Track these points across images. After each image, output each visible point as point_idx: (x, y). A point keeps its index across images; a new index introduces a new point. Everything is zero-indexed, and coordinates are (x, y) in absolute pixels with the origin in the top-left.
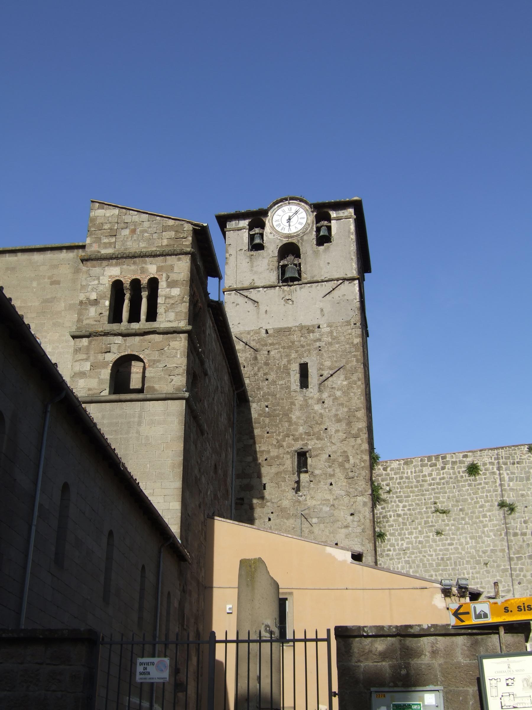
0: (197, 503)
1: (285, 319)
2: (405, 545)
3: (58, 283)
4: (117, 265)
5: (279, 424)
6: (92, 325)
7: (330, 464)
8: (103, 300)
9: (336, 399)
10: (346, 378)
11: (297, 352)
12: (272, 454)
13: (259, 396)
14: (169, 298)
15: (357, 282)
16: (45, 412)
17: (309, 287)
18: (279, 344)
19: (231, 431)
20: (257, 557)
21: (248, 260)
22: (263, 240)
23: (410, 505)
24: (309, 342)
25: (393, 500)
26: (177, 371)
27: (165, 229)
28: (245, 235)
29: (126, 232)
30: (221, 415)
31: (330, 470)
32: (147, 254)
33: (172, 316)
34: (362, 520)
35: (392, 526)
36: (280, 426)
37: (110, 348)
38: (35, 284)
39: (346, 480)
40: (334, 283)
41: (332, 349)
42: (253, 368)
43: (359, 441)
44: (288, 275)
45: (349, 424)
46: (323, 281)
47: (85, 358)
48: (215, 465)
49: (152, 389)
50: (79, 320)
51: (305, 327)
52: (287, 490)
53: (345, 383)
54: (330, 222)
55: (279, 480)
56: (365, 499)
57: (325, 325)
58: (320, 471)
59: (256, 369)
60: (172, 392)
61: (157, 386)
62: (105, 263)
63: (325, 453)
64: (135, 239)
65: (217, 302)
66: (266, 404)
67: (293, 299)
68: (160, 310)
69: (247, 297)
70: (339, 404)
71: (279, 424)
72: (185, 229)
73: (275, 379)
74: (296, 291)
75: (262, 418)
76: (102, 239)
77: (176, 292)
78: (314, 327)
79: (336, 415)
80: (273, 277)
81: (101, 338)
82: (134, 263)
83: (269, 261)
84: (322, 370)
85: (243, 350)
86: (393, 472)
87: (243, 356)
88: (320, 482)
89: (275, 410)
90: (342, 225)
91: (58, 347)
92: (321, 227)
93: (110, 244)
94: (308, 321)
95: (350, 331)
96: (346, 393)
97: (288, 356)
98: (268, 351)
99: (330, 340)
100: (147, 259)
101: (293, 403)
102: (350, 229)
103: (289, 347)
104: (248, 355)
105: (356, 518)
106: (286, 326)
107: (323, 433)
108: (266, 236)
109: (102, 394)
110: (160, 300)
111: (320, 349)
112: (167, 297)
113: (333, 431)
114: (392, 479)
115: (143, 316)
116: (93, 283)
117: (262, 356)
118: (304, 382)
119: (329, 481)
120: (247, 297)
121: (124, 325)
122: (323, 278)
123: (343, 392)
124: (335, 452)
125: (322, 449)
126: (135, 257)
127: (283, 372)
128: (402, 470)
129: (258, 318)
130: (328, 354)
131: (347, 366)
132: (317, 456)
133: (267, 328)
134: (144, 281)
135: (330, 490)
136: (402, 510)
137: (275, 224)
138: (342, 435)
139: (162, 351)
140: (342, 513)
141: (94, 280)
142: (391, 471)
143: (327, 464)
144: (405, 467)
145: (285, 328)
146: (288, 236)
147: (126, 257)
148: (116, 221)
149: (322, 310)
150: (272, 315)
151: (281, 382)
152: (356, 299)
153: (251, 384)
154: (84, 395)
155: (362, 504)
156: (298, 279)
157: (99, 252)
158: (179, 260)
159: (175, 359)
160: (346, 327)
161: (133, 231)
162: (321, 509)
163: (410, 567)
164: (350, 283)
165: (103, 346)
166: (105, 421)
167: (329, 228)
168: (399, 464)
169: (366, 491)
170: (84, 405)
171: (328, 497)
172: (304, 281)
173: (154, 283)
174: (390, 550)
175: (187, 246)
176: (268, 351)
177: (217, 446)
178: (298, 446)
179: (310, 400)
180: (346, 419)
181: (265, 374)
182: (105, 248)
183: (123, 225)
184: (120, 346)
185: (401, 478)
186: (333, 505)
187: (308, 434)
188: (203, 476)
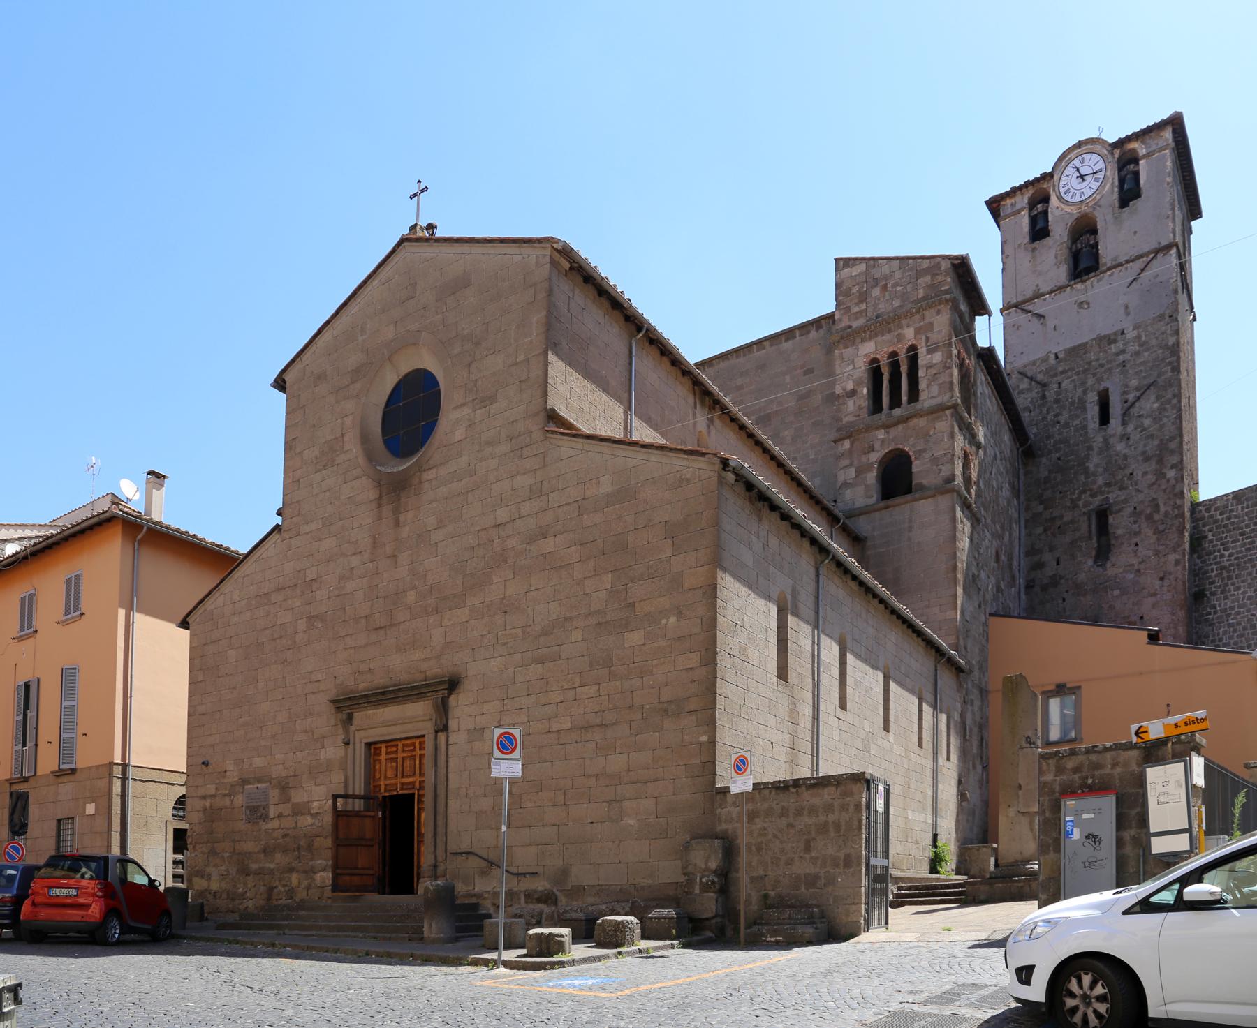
0: (976, 604)
2: (1229, 605)
11: (1094, 375)
12: (1065, 519)
23: (1238, 552)
27: (920, 274)
29: (876, 292)
31: (1135, 527)
38: (788, 378)
44: (1082, 266)
46: (1128, 262)
47: (835, 648)
51: (1105, 337)
53: (1156, 405)
61: (925, 482)
65: (988, 349)
68: (922, 385)
77: (937, 357)
93: (861, 312)
94: (1106, 327)
96: (1156, 420)
97: (1083, 384)
101: (1090, 448)
102: (1165, 166)
103: (1085, 371)
105: (1166, 582)
110: (921, 373)
112: (929, 367)
113: (1140, 474)
115: (904, 398)
118: (1104, 419)
121: (883, 416)
124: (1142, 502)
125: (1125, 501)
127: (1077, 409)
132: (1119, 511)
137: (1062, 190)
151: (1076, 422)
157: (850, 327)
158: (938, 312)
161: (885, 288)
171: (1134, 561)
178: (1097, 501)
181: (1056, 416)
182: (857, 319)
184: (883, 441)
186: (1138, 571)
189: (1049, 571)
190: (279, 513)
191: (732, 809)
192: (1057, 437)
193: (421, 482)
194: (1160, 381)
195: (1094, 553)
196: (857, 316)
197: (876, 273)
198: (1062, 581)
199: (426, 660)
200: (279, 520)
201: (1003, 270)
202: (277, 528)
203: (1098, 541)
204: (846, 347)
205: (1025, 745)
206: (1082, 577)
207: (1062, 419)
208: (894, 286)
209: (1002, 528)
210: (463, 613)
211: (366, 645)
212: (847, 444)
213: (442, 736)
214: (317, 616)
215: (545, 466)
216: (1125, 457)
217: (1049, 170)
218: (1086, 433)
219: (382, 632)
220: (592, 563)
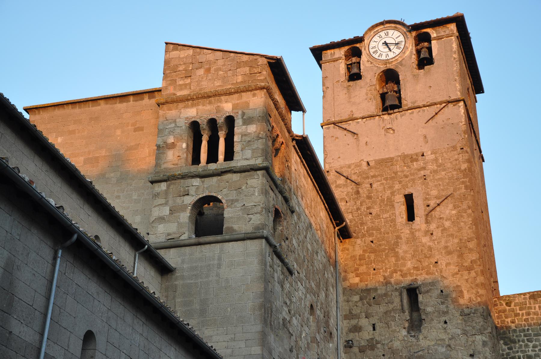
0: (287, 347)
1: (386, 150)
3: (141, 129)
4: (193, 106)
5: (385, 259)
6: (170, 169)
7: (443, 301)
8: (180, 143)
9: (444, 230)
10: (455, 207)
11: (400, 182)
12: (379, 292)
13: (363, 231)
14: (245, 135)
15: (462, 103)
16: (55, 258)
17: (410, 114)
18: (381, 175)
19: (332, 269)
21: (345, 91)
22: (360, 69)
24: (412, 171)
25: (521, 339)
27: (239, 65)
28: (342, 66)
29: (201, 72)
30: (317, 253)
31: (443, 307)
32: (222, 93)
33: (248, 153)
36: (386, 261)
37: (188, 190)
38: (118, 132)
39: (461, 317)
40: (437, 108)
41: (438, 177)
42: (356, 202)
43: (473, 274)
45: (461, 256)
46: (424, 106)
47: (163, 202)
48: (312, 306)
49: (231, 229)
50: (157, 165)
51: (408, 156)
52: (398, 330)
53: (454, 212)
54: (431, 43)
55: (389, 319)
56: (484, 338)
57: (429, 153)
58: (433, 308)
59: (358, 203)
60: (250, 232)
61: (236, 227)
62: (181, 105)
63: (437, 289)
64: (210, 78)
66: (371, 239)
67: (394, 128)
68: (237, 148)
69: (345, 129)
70: (449, 235)
71: (385, 259)
72: (259, 64)
73: (379, 213)
74: (396, 119)
75: (367, 255)
76: (177, 81)
77: (252, 129)
78: (417, 156)
79: (446, 247)
80: (373, 105)
81: (178, 181)
82: (210, 103)
83: (367, 90)
84: (429, 200)
85: (344, 185)
86: (518, 308)
87: (159, 184)
88: (432, 320)
89: (380, 245)
90: (444, 46)
91: (143, 193)
92: (421, 49)
93: (186, 85)
95: (456, 156)
97: (391, 187)
98: (371, 184)
99: (436, 168)
100: (223, 98)
101: (399, 237)
102: (452, 48)
103: (392, 178)
104: (349, 189)
106: (387, 157)
107: (433, 266)
108: (363, 64)
109: (182, 238)
110: (236, 139)
111: (425, 178)
112: (243, 135)
114: (517, 315)
115: (221, 156)
116: (170, 126)
117: (364, 190)
118: (411, 217)
119: (444, 319)
120: (345, 129)
122: (425, 103)
123: (453, 222)
126: (209, 97)
128: (528, 305)
129: (358, 150)
130: (434, 182)
131: (455, 194)
132: (428, 292)
133: (368, 160)
134: (221, 121)
135: (445, 329)
136: (532, 351)
137: (372, 51)
138: (453, 268)
139: (240, 190)
140: (460, 354)
141: (171, 123)
142: (515, 306)
143: (439, 300)
144: (532, 301)
145: (388, 159)
146: (386, 62)
147: (203, 97)
148: (190, 61)
149: (425, 137)
150: (373, 146)
151: (385, 216)
152: (462, 122)
153: (354, 220)
154: (164, 240)
155: (481, 343)
156: (399, 106)
157: (174, 94)
158: (254, 95)
159: (253, 197)
160: (453, 152)
161: (208, 70)
162: (436, 350)
164: (454, 105)
165: (182, 189)
166: (185, 266)
167: (430, 49)
168: (524, 299)
169: (485, 329)
170: (158, 251)
171: (443, 336)
172: (404, 107)
173: (230, 121)
176: (371, 184)
177: (313, 286)
179: (417, 233)
180: (457, 251)
181: (368, 208)
182: (181, 89)
183: (197, 65)
184: (198, 188)
185: (528, 314)
187: (416, 268)
188: (294, 318)
189: (367, 334)
192: (370, 225)
195: (407, 325)
196: (181, 87)
198: (379, 346)
201: (324, 97)
203: (411, 316)
204: (170, 109)
206: (397, 344)
207: (374, 211)
208: (219, 69)
209: (318, 286)
212: (163, 186)
216: (430, 249)
217: (361, 35)
218: (395, 225)
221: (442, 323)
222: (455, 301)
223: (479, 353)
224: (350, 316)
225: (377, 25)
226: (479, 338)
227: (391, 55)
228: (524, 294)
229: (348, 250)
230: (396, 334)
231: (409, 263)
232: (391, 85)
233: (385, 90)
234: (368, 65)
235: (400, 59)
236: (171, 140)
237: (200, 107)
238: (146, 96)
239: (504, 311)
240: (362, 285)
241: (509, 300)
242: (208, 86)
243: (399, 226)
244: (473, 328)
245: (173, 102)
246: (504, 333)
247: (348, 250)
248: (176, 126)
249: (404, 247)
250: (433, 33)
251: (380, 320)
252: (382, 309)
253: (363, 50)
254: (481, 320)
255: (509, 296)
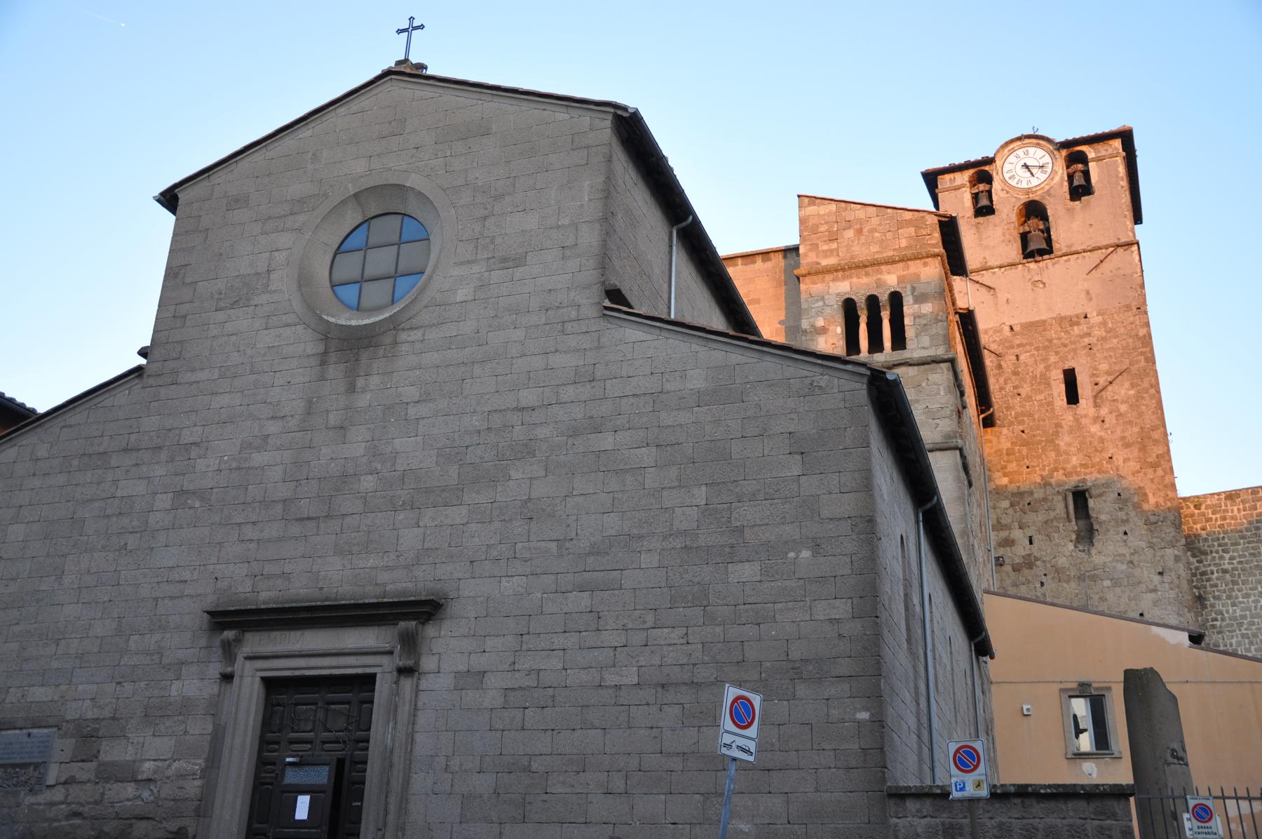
2: (1238, 613)
4: (844, 278)
9: (1120, 415)
11: (1057, 353)
12: (1036, 496)
20: (1148, 666)
21: (973, 231)
23: (1240, 556)
26: (943, 413)
27: (901, 224)
29: (850, 234)
31: (1121, 515)
34: (1176, 581)
35: (1216, 586)
44: (1033, 246)
45: (1143, 449)
53: (1132, 392)
62: (828, 277)
66: (1021, 428)
68: (910, 333)
77: (927, 308)
79: (1123, 438)
80: (1013, 251)
82: (867, 274)
88: (1108, 530)
93: (831, 251)
97: (1045, 360)
101: (1058, 425)
103: (1045, 348)
105: (1166, 578)
112: (917, 317)
115: (887, 343)
118: (1072, 396)
119: (1123, 529)
126: (866, 266)
132: (1100, 495)
133: (1012, 323)
134: (884, 298)
137: (1007, 176)
138: (1134, 465)
143: (1116, 506)
144: (1229, 503)
146: (1028, 191)
147: (858, 267)
151: (1039, 397)
157: (818, 263)
158: (925, 264)
161: (860, 231)
163: (1251, 643)
167: (1086, 174)
172: (1056, 253)
174: (1216, 620)
175: (933, 246)
181: (1015, 387)
182: (826, 257)
185: (1224, 518)
189: (1022, 549)
190: (143, 353)
191: (916, 821)
192: (1019, 409)
193: (396, 343)
194: (1134, 369)
195: (1074, 537)
196: (827, 254)
197: (849, 215)
198: (1038, 563)
199: (388, 568)
200: (143, 361)
202: (138, 370)
204: (815, 283)
205: (1170, 759)
206: (1062, 561)
208: (872, 231)
210: (458, 514)
211: (279, 540)
213: (407, 684)
214: (194, 493)
215: (598, 348)
216: (1102, 440)
217: (991, 155)
219: (312, 524)
220: (673, 472)
221: (1121, 535)
222: (1137, 507)
223: (1170, 570)
224: (999, 526)
225: (1012, 141)
226: (1170, 552)
227: (1035, 182)
228: (1219, 494)
229: (991, 442)
230: (1060, 549)
231: (1074, 458)
232: (1034, 222)
233: (1027, 229)
234: (1003, 194)
235: (1047, 188)
236: (820, 322)
237: (855, 280)
238: (759, 259)
239: (1192, 515)
240: (1012, 488)
241: (1197, 502)
242: (862, 252)
243: (1058, 411)
244: (1162, 539)
245: (817, 273)
246: (1193, 542)
247: (991, 442)
248: (825, 305)
249: (1067, 438)
250: (1090, 152)
251: (1039, 531)
252: (1041, 517)
253: (994, 175)
254: (1172, 530)
255: (1198, 497)
